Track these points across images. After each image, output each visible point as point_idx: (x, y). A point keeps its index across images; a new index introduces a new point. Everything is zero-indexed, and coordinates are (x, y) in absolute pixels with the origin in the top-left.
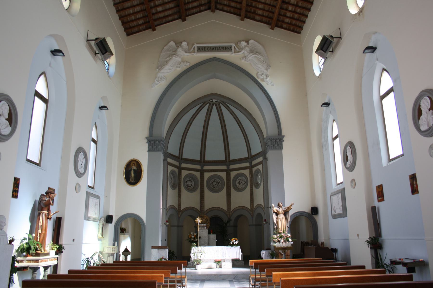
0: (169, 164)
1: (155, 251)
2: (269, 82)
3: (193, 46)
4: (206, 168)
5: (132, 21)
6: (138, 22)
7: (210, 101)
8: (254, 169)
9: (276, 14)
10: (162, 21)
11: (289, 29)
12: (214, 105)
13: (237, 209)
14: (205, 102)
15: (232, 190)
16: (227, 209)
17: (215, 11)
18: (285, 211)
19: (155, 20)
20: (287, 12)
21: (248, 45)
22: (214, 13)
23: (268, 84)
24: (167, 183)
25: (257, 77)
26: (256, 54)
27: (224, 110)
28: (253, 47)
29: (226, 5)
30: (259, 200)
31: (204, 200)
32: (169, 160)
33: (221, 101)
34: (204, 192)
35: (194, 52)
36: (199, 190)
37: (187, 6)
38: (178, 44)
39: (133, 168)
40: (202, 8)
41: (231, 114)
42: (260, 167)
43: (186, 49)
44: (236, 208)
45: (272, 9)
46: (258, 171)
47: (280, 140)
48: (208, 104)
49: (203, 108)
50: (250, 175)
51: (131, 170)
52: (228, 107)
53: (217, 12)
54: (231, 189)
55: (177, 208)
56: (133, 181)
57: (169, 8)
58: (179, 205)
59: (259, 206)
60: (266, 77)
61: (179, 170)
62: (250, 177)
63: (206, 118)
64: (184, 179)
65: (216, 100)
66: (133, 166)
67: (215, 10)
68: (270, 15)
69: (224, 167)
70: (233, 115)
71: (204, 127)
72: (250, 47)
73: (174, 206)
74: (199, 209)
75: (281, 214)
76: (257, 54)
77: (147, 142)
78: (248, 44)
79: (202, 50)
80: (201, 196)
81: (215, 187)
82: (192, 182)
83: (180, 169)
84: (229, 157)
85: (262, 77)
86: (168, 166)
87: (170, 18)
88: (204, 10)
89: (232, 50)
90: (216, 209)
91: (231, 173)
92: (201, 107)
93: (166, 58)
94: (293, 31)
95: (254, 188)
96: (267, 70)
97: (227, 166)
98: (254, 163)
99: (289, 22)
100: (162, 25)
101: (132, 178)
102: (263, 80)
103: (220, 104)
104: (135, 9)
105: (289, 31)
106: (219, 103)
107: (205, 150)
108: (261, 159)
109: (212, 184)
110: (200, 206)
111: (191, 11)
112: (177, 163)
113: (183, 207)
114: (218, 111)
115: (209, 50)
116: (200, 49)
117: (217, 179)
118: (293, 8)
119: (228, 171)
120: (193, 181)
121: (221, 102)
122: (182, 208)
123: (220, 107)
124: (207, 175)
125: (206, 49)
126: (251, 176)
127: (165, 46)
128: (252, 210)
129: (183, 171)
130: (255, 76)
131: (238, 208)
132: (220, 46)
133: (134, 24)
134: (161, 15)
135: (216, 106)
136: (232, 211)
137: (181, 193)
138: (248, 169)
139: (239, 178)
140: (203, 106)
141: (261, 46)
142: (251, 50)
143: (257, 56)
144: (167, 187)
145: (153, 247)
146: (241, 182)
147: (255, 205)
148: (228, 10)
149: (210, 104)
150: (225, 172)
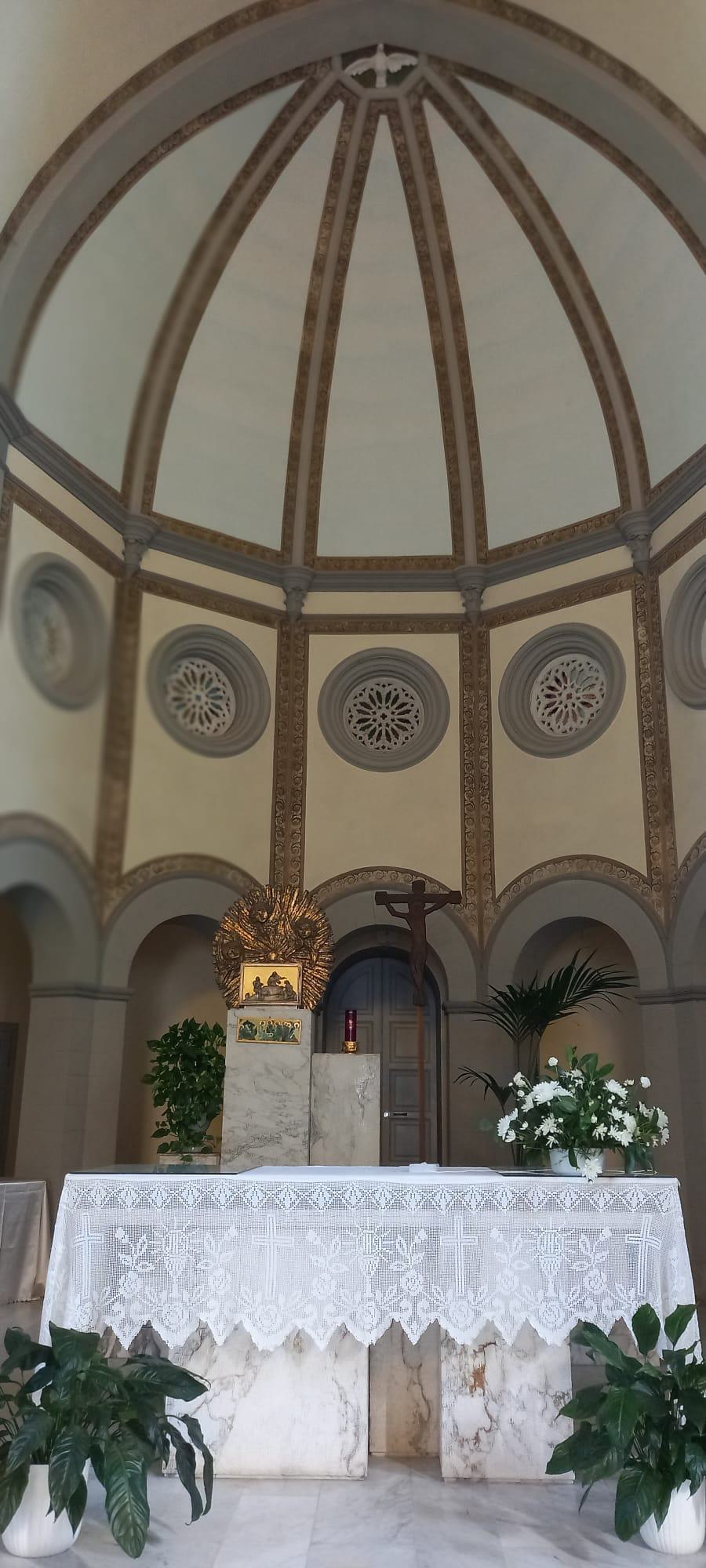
4: (319, 603)
13: (535, 879)
15: (502, 747)
31: (303, 814)
33: (436, 60)
34: (303, 763)
36: (264, 749)
44: (531, 871)
50: (641, 630)
54: (490, 744)
62: (638, 645)
69: (448, 603)
71: (310, 315)
80: (278, 790)
81: (380, 734)
82: (220, 693)
107: (315, 489)
109: (368, 701)
110: (273, 856)
113: (136, 853)
114: (408, 180)
117: (399, 684)
126: (643, 639)
136: (504, 893)
138: (622, 589)
139: (554, 664)
150: (451, 631)
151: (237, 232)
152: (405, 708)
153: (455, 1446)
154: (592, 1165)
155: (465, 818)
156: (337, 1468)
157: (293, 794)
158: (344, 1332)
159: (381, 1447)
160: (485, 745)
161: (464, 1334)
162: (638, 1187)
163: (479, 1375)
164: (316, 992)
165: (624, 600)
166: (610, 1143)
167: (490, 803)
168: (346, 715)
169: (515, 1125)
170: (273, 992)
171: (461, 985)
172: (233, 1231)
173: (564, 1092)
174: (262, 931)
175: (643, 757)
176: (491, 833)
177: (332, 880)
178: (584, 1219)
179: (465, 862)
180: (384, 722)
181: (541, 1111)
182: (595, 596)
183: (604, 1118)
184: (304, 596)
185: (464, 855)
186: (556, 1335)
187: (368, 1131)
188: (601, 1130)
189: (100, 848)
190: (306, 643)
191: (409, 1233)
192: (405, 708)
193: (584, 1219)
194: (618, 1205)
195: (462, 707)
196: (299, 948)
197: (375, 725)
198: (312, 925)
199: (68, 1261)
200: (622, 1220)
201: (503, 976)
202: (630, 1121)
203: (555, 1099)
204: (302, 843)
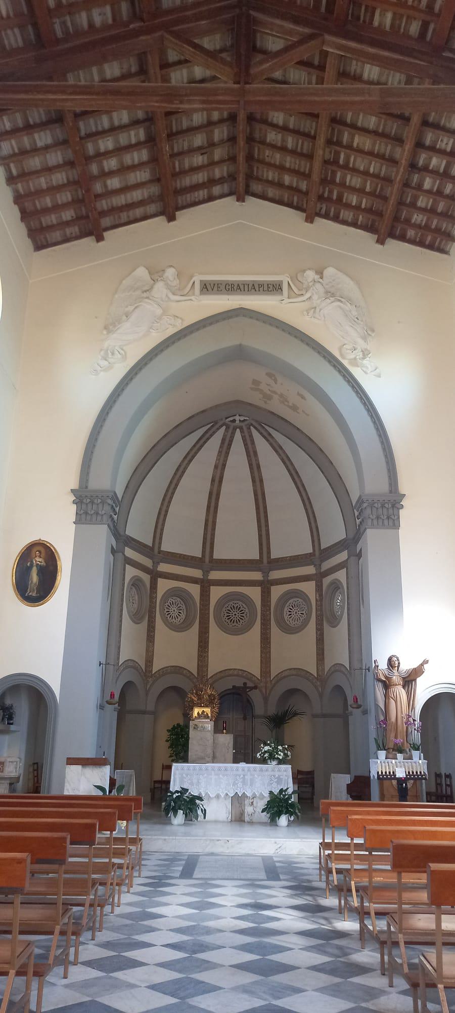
0: (129, 561)
1: (74, 771)
2: (369, 367)
3: (191, 279)
4: (215, 575)
5: (46, 211)
6: (61, 217)
7: (227, 420)
8: (327, 581)
9: (392, 201)
10: (120, 217)
11: (421, 243)
12: (238, 430)
14: (216, 423)
15: (274, 630)
16: (261, 675)
17: (245, 200)
18: (407, 679)
19: (103, 214)
20: (419, 193)
21: (321, 280)
22: (244, 203)
23: (366, 373)
24: (122, 605)
25: (341, 355)
26: (340, 301)
27: (261, 445)
28: (333, 286)
29: (271, 183)
30: (338, 653)
32: (129, 552)
35: (194, 294)
36: (196, 627)
37: (178, 182)
38: (156, 274)
39: (36, 561)
40: (216, 190)
41: (276, 451)
42: (341, 575)
43: (176, 286)
45: (382, 189)
46: (336, 586)
47: (393, 506)
48: (224, 427)
49: (211, 436)
50: (317, 595)
51: (32, 566)
52: (270, 434)
53: (251, 201)
55: (143, 667)
56: (34, 594)
57: (135, 182)
58: (149, 661)
59: (338, 667)
60: (361, 356)
61: (151, 578)
62: (316, 600)
63: (219, 460)
64: (161, 600)
65: (242, 418)
66: (36, 557)
67: (246, 197)
68: (377, 205)
69: (257, 576)
70: (279, 455)
71: (213, 480)
72: (327, 284)
73: (137, 663)
74: (195, 671)
75: (396, 685)
76: (342, 300)
77: (74, 502)
78: (322, 278)
79: (213, 290)
83: (155, 576)
84: (269, 553)
85: (352, 356)
86: (125, 566)
87: (139, 212)
88: (222, 196)
89: (282, 291)
90: (236, 673)
91: (273, 588)
92: (206, 432)
93: (127, 307)
94: (431, 247)
95: (326, 626)
96: (364, 338)
97: (263, 573)
98: (327, 565)
99: (429, 208)
100: (121, 229)
101: (33, 585)
102: (354, 362)
103: (252, 427)
104: (53, 177)
105: (421, 249)
106: (248, 424)
107: (213, 535)
108: (343, 556)
110: (198, 665)
111: (188, 195)
112: (147, 562)
113: (156, 667)
114: (246, 445)
115: (229, 289)
116: (208, 288)
118: (436, 182)
119: (266, 586)
120: (184, 606)
121: (254, 423)
122: (155, 669)
123: (251, 436)
124: (217, 593)
125: (223, 287)
127: (124, 279)
128: (321, 679)
129: (160, 581)
130: (337, 354)
131: (286, 673)
132: (254, 281)
133: (52, 221)
134: (120, 200)
135: (242, 432)
137: (154, 632)
138: (312, 580)
139: (291, 601)
140: (211, 432)
141: (352, 283)
142: (327, 292)
143: (342, 305)
144: (121, 616)
145: (72, 761)
146: (294, 610)
147: (328, 665)
148: (277, 198)
149: (228, 427)
151: (190, 461)
152: (242, 612)
153: (247, 816)
154: (274, 763)
155: (262, 652)
156: (225, 820)
157: (205, 643)
158: (227, 794)
159: (233, 819)
160: (269, 627)
161: (249, 794)
162: (283, 767)
163: (252, 803)
164: (215, 714)
165: (312, 584)
166: (278, 758)
167: (270, 648)
168: (222, 614)
169: (260, 755)
170: (202, 715)
171: (259, 709)
172: (206, 775)
173: (270, 748)
174: (200, 697)
175: (317, 637)
176: (270, 657)
177: (218, 673)
178: (272, 773)
179: (261, 667)
180: (233, 615)
181: (266, 752)
182: (304, 581)
183: (277, 754)
184: (209, 573)
185: (261, 665)
186: (266, 795)
187: (231, 757)
188: (277, 756)
189: (146, 666)
190: (210, 589)
191: (240, 776)
192: (242, 612)
193: (272, 773)
194: (279, 771)
195: (261, 613)
196: (210, 703)
197: (232, 618)
198: (214, 696)
199: (174, 781)
200: (280, 773)
201: (272, 710)
202: (282, 754)
203: (268, 750)
204: (208, 660)
